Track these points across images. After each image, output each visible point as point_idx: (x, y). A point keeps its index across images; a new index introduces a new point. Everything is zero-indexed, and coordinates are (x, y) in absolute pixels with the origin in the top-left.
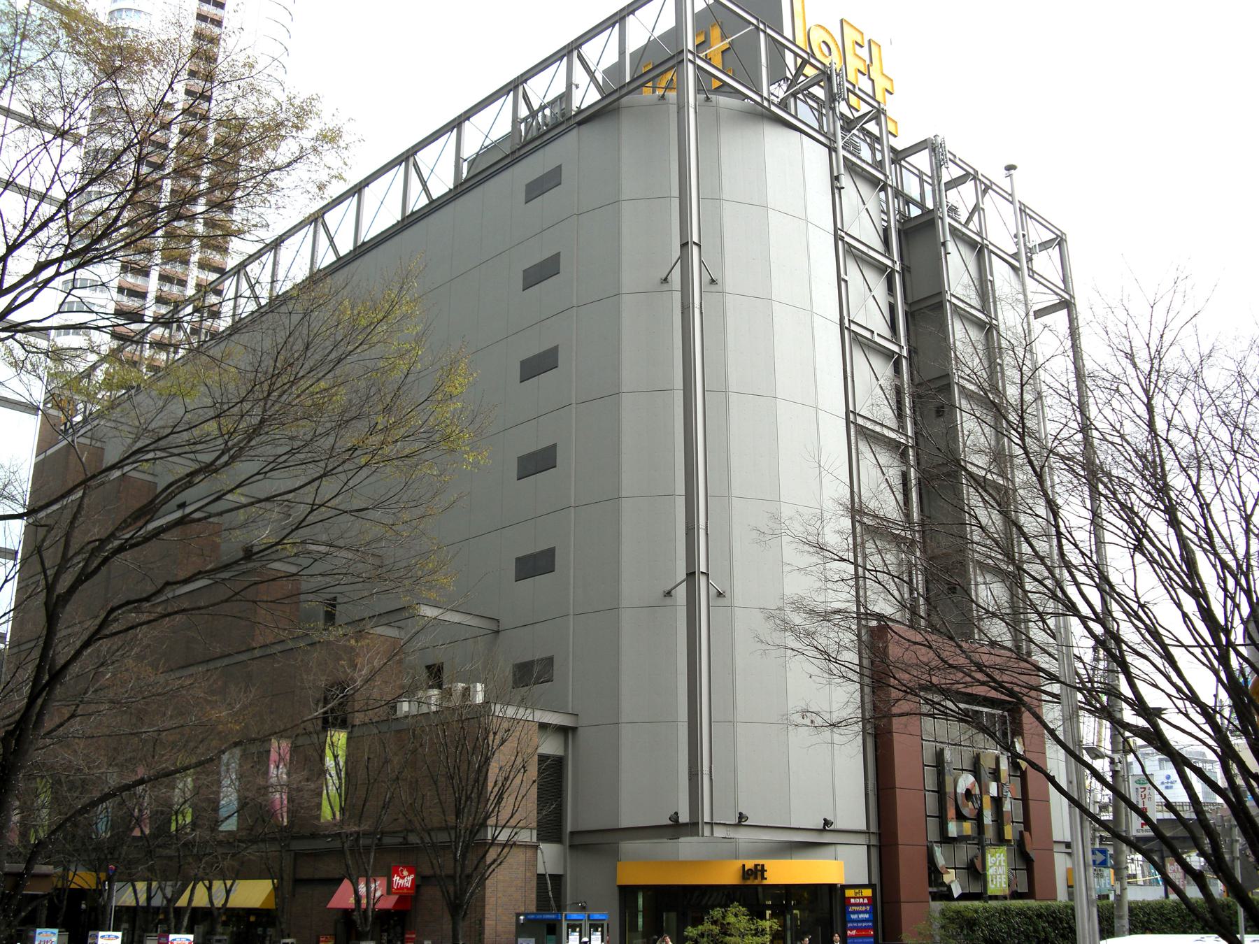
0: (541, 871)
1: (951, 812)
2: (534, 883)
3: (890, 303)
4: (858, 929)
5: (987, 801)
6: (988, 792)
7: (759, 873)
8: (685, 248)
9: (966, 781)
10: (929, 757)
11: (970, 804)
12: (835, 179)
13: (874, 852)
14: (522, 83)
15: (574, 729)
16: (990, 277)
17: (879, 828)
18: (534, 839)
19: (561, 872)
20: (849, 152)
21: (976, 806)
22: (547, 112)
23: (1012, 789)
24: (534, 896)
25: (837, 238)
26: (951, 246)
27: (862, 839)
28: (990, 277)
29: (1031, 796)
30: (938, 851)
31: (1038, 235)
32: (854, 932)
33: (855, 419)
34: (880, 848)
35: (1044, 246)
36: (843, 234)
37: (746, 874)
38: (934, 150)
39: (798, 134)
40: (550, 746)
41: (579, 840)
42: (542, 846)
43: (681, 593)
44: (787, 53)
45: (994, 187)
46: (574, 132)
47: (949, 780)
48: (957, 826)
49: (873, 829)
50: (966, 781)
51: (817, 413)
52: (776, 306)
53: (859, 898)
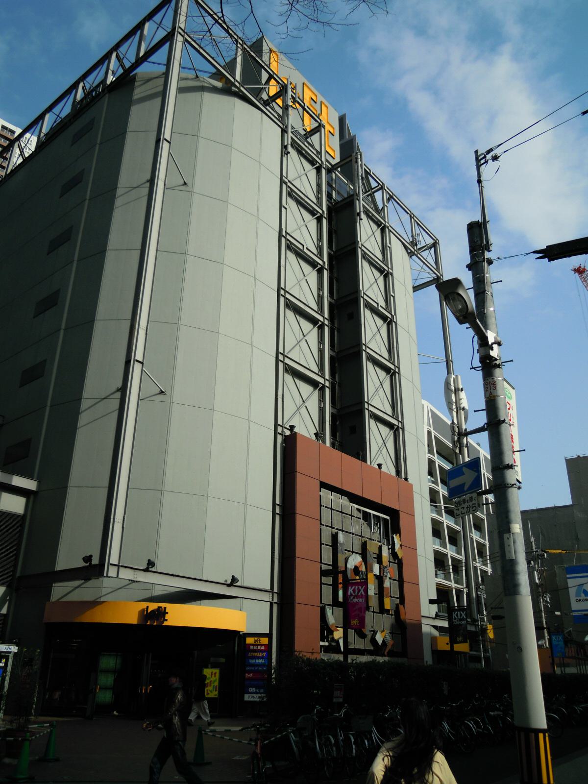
4: (254, 672)
5: (371, 577)
6: (372, 571)
9: (355, 560)
10: (327, 538)
12: (284, 147)
16: (388, 244)
20: (294, 134)
23: (392, 571)
25: (282, 182)
26: (363, 216)
27: (267, 597)
29: (405, 579)
30: (329, 611)
32: (251, 675)
34: (281, 605)
44: (263, 71)
45: (394, 197)
50: (355, 560)
52: (230, 207)
53: (258, 645)
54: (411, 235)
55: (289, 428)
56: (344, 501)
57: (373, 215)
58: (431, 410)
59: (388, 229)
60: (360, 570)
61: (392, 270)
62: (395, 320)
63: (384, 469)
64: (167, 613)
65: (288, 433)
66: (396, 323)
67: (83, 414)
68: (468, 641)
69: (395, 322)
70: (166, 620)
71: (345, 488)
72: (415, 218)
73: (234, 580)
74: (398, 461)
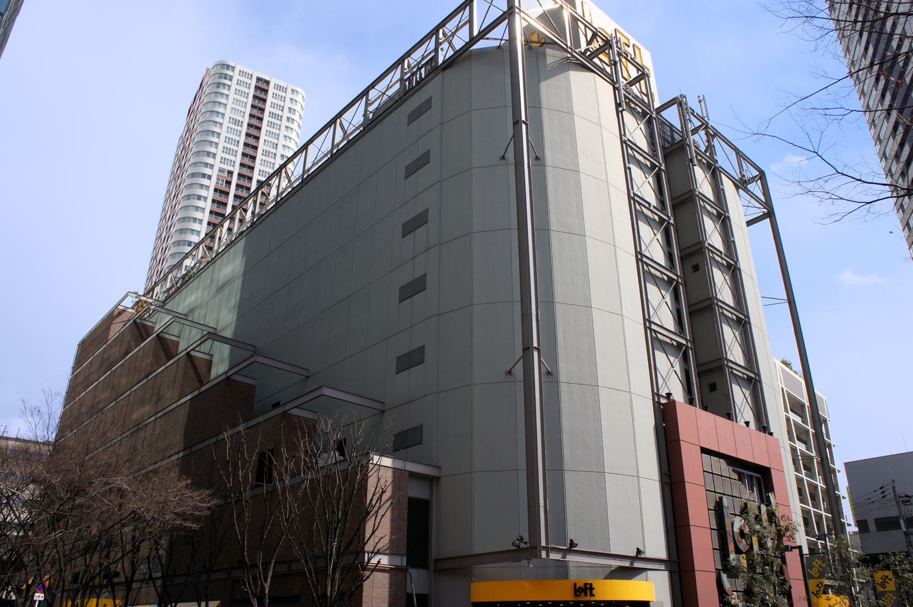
1: (731, 547)
7: (588, 591)
8: (517, 125)
9: (738, 523)
11: (744, 540)
12: (618, 105)
14: (407, 58)
15: (438, 479)
18: (405, 564)
21: (748, 543)
22: (423, 70)
33: (650, 325)
37: (578, 591)
38: (680, 105)
39: (593, 74)
42: (412, 571)
43: (519, 370)
46: (441, 74)
47: (727, 521)
50: (738, 523)
51: (615, 250)
54: (739, 171)
55: (666, 396)
58: (780, 367)
59: (719, 170)
60: (745, 532)
61: (728, 213)
62: (739, 267)
64: (594, 589)
65: (663, 401)
66: (739, 269)
67: (644, 64)
70: (594, 596)
72: (740, 153)
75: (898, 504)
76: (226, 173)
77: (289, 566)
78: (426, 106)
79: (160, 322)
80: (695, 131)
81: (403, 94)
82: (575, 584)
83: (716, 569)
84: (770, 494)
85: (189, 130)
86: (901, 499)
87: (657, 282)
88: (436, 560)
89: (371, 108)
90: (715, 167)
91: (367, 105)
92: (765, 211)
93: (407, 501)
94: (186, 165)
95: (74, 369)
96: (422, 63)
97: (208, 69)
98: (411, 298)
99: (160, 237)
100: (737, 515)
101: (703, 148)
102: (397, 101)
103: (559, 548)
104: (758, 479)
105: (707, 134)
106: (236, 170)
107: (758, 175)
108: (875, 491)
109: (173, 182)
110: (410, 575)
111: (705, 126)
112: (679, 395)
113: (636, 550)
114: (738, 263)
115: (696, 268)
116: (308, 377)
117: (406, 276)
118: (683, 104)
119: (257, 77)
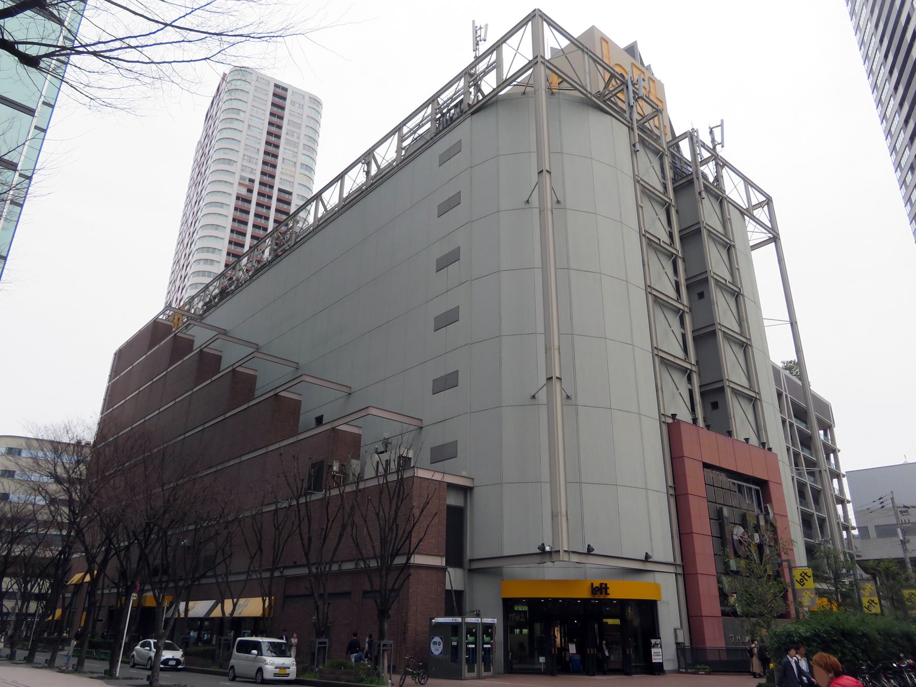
0: (448, 587)
2: (444, 596)
3: (676, 281)
7: (603, 590)
13: (681, 579)
15: (470, 489)
16: (728, 216)
17: (674, 484)
18: (444, 564)
19: (462, 589)
23: (768, 536)
24: (443, 605)
25: (648, 293)
26: (704, 194)
27: (671, 569)
28: (737, 267)
31: (757, 198)
34: (684, 576)
35: (760, 205)
36: (639, 179)
38: (691, 139)
40: (453, 500)
41: (476, 565)
46: (469, 119)
48: (736, 562)
49: (679, 562)
50: (739, 531)
56: (723, 477)
57: (650, 143)
62: (742, 293)
63: (750, 442)
65: (670, 421)
68: (284, 637)
69: (742, 295)
70: (609, 594)
71: (722, 466)
73: (647, 557)
74: (759, 429)
75: (896, 514)
76: (247, 181)
77: (340, 566)
78: (456, 149)
79: (200, 336)
80: (705, 162)
81: (434, 134)
82: (592, 584)
83: (717, 573)
84: (768, 505)
85: (207, 136)
86: (899, 509)
87: (665, 314)
88: (471, 561)
89: (405, 144)
90: (723, 198)
91: (402, 139)
92: (770, 235)
93: (446, 508)
94: (207, 172)
95: (111, 377)
96: (452, 105)
97: (225, 75)
98: (445, 328)
99: (182, 242)
100: (737, 524)
101: (711, 179)
102: (429, 141)
103: (829, 525)
104: (757, 491)
105: (717, 164)
106: (257, 178)
107: (766, 200)
108: (874, 502)
109: (193, 187)
110: (449, 573)
111: (715, 157)
112: (684, 415)
113: (645, 555)
114: (741, 289)
115: (701, 295)
116: (350, 394)
117: (440, 307)
118: (694, 138)
119: (275, 84)
